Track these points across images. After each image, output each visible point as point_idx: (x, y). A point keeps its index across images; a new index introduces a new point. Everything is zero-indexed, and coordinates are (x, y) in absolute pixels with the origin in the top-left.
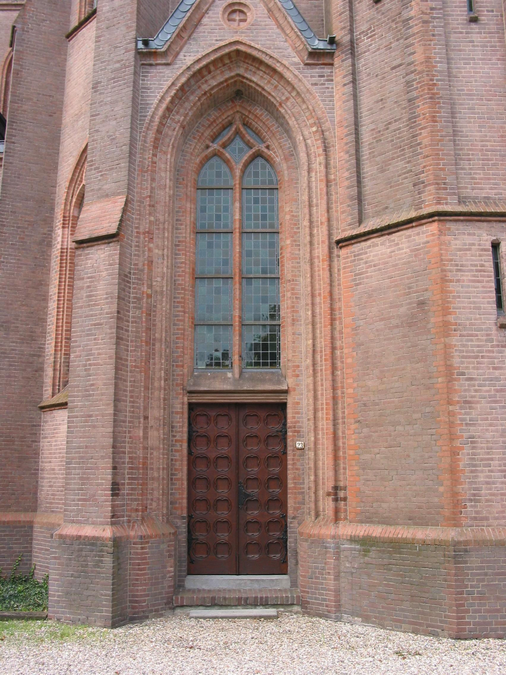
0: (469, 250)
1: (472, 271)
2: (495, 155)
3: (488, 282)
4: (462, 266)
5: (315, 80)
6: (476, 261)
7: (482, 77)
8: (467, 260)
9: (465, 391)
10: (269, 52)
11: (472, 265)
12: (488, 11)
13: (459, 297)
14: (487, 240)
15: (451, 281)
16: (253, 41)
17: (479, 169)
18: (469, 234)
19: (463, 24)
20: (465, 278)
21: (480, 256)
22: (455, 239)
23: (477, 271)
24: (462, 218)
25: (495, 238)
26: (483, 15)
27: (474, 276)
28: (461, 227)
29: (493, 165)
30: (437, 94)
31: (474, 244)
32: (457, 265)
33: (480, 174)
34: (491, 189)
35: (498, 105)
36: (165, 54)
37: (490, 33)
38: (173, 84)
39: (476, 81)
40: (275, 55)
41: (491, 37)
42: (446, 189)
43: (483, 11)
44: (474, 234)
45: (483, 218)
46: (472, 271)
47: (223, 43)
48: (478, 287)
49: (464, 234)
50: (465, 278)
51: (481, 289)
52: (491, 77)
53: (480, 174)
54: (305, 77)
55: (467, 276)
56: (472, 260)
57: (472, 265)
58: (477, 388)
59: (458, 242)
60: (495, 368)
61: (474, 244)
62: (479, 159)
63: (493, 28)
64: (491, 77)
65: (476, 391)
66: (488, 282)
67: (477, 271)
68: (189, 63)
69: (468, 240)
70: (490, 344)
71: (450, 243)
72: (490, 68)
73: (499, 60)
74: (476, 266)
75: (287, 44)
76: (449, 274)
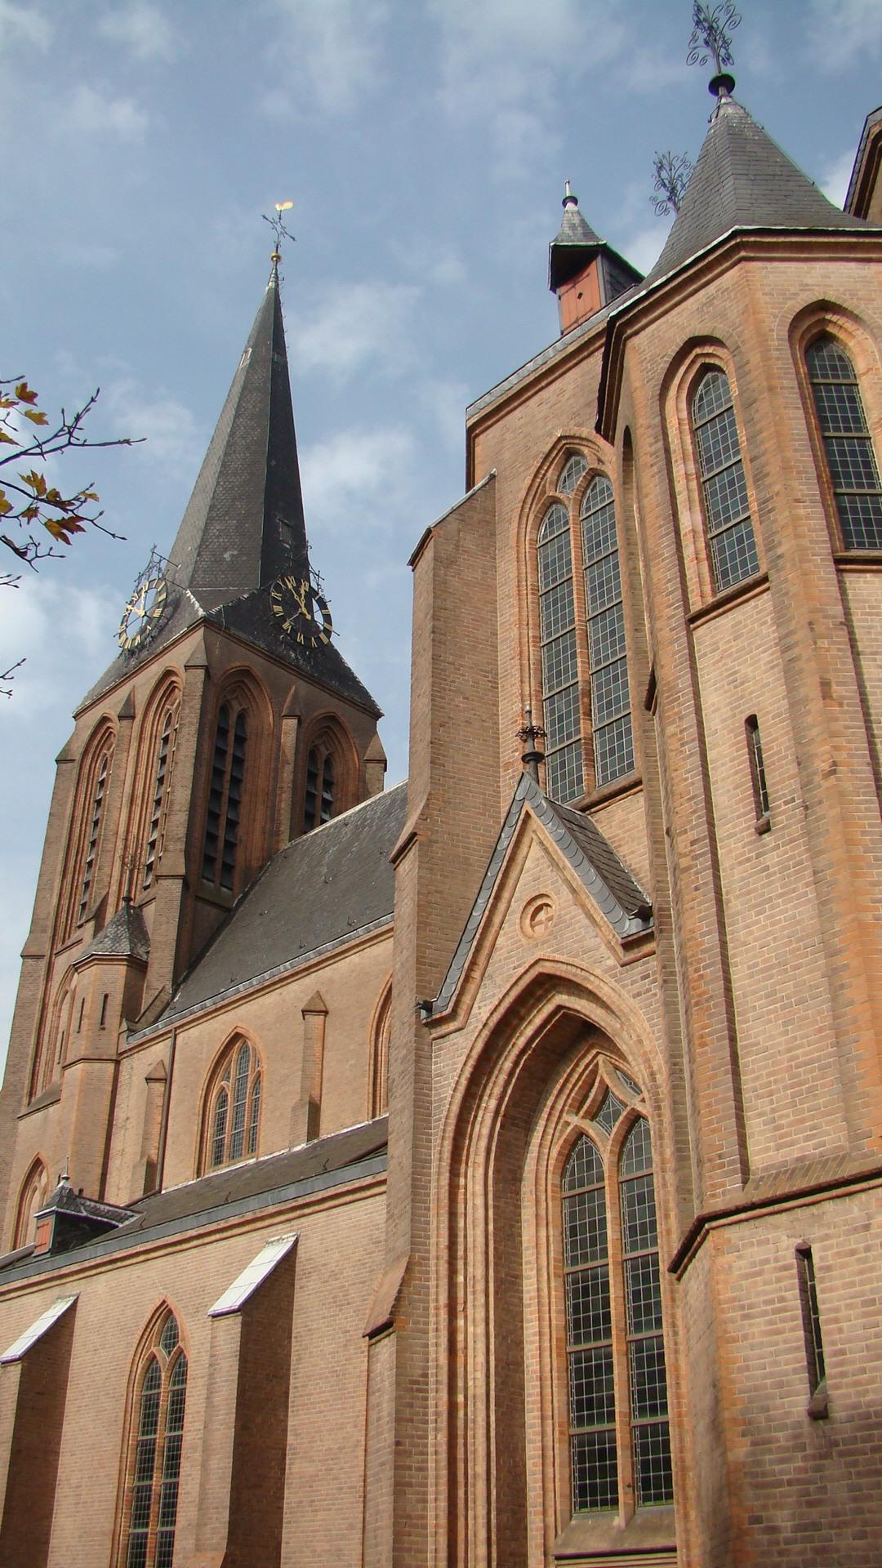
0: (760, 1273)
1: (765, 1313)
2: (812, 1070)
3: (792, 1329)
4: (751, 1306)
5: (636, 988)
6: (771, 1292)
7: (784, 928)
8: (758, 1294)
9: (763, 1553)
10: (577, 962)
11: (766, 1302)
12: (786, 803)
13: (747, 1368)
14: (787, 1247)
15: (734, 1340)
16: (557, 950)
17: (786, 1107)
18: (760, 1243)
19: (750, 843)
20: (755, 1330)
21: (779, 1280)
22: (739, 1257)
23: (775, 1311)
24: (743, 1216)
25: (800, 1241)
26: (780, 814)
27: (771, 1323)
28: (747, 1233)
29: (809, 1091)
30: (705, 993)
31: (767, 1261)
32: (742, 1307)
33: (788, 1116)
34: (807, 1139)
35: (812, 971)
36: (453, 1016)
37: (791, 841)
38: (468, 1057)
39: (775, 939)
40: (584, 965)
41: (793, 849)
42: (722, 1166)
43: (779, 806)
44: (767, 1241)
45: (777, 1207)
46: (765, 1313)
47: (522, 970)
48: (777, 1344)
49: (752, 1244)
50: (755, 1330)
51: (782, 1346)
52: (798, 923)
53: (788, 1116)
54: (624, 987)
55: (758, 1326)
56: (766, 1293)
57: (766, 1302)
58: (783, 1546)
59: (742, 1263)
60: (810, 1504)
61: (767, 1261)
62: (785, 1088)
63: (796, 829)
64: (798, 923)
65: (780, 1553)
66: (792, 1329)
67: (775, 1311)
68: (485, 1017)
69: (757, 1253)
70: (800, 1455)
71: (730, 1267)
72: (795, 907)
73: (807, 885)
74: (771, 1302)
75: (598, 940)
76: (730, 1326)
